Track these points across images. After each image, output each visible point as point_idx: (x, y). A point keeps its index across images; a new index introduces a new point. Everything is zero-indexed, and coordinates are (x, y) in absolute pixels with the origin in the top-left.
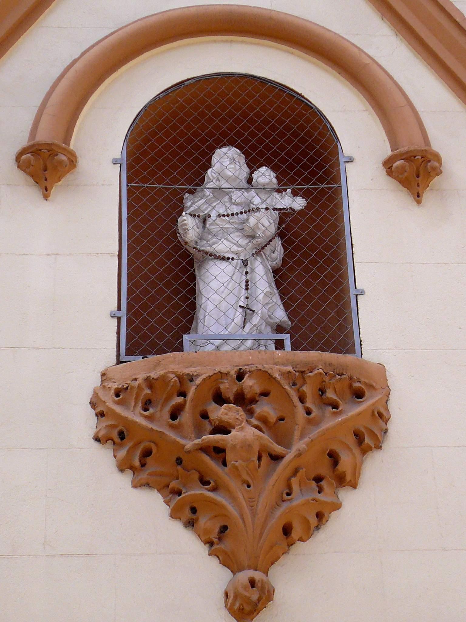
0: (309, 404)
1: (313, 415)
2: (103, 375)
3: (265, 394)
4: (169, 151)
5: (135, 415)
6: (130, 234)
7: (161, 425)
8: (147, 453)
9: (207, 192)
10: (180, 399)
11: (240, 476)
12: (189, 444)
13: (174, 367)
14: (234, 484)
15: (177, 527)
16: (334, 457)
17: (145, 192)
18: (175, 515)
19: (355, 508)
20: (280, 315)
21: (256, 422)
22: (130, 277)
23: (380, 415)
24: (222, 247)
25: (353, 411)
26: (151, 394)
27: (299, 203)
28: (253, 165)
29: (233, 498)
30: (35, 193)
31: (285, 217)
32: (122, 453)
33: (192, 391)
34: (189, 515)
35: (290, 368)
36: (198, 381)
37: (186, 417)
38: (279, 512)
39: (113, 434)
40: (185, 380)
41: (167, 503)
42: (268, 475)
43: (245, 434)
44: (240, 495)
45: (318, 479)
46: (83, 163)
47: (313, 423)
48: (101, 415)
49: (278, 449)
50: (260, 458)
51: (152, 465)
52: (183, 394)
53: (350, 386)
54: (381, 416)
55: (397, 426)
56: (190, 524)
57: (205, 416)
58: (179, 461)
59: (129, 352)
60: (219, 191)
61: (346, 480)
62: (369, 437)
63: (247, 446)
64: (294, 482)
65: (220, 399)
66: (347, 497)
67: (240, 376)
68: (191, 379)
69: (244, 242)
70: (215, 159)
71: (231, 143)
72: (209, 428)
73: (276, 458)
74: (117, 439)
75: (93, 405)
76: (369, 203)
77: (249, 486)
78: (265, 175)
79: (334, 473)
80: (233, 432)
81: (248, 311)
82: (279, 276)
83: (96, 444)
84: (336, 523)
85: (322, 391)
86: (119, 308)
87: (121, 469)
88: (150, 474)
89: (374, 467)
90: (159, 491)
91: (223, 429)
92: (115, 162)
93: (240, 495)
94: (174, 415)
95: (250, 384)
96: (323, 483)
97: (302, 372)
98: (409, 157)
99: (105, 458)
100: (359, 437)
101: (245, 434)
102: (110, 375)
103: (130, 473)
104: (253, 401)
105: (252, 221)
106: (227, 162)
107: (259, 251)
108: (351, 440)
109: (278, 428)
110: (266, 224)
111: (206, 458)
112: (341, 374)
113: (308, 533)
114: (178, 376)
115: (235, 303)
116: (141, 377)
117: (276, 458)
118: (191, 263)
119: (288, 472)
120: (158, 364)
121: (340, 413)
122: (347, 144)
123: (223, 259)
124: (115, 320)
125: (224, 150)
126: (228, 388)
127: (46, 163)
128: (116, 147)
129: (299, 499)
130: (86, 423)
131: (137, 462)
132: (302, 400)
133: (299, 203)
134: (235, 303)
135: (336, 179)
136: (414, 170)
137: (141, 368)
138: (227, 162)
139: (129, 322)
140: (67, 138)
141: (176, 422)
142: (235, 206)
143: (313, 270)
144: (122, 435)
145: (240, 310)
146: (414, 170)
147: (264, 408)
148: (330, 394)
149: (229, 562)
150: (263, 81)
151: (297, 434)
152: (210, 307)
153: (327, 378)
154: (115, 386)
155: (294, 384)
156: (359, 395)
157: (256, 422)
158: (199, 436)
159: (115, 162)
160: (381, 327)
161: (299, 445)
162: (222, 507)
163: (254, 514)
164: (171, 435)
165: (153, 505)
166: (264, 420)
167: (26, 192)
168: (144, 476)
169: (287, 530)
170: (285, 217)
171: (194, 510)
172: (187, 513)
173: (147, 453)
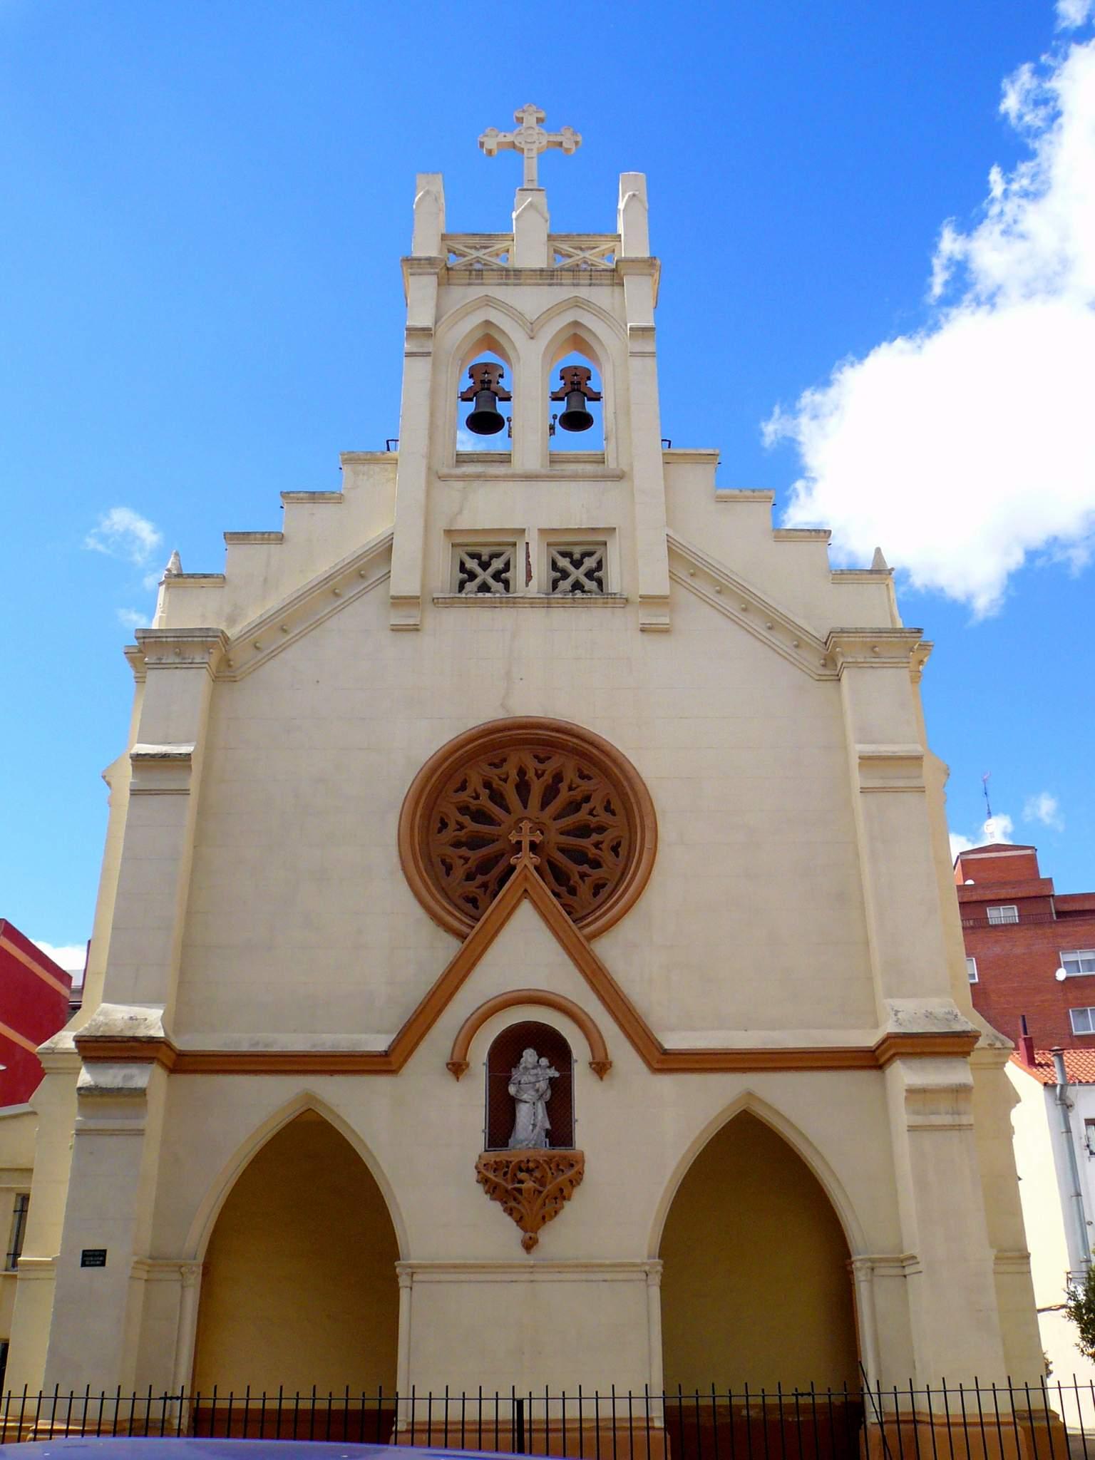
5: (491, 1175)
7: (499, 1180)
15: (505, 1215)
19: (570, 1209)
20: (548, 1126)
24: (525, 1097)
26: (497, 1167)
27: (557, 1075)
28: (540, 1056)
34: (510, 1211)
37: (509, 1176)
39: (484, 1181)
40: (508, 1163)
43: (529, 1185)
46: (472, 1065)
54: (581, 1173)
56: (511, 1214)
60: (526, 1068)
62: (576, 1181)
65: (522, 1171)
66: (567, 1204)
73: (540, 1192)
79: (561, 1196)
81: (534, 1125)
84: (562, 1214)
87: (487, 1193)
89: (578, 1193)
91: (521, 1182)
95: (531, 1165)
98: (598, 1064)
99: (480, 1189)
100: (571, 1181)
101: (529, 1185)
106: (529, 1056)
110: (543, 1085)
113: (551, 1218)
115: (530, 1119)
117: (540, 1192)
122: (575, 1055)
126: (524, 1166)
130: (473, 1175)
133: (557, 1075)
134: (530, 1119)
136: (601, 1067)
137: (493, 1156)
138: (529, 1056)
142: (532, 1072)
143: (560, 1102)
146: (601, 1067)
147: (537, 1174)
149: (525, 1229)
156: (572, 1165)
160: (583, 1137)
161: (549, 1187)
165: (497, 1207)
167: (450, 1077)
169: (544, 1218)
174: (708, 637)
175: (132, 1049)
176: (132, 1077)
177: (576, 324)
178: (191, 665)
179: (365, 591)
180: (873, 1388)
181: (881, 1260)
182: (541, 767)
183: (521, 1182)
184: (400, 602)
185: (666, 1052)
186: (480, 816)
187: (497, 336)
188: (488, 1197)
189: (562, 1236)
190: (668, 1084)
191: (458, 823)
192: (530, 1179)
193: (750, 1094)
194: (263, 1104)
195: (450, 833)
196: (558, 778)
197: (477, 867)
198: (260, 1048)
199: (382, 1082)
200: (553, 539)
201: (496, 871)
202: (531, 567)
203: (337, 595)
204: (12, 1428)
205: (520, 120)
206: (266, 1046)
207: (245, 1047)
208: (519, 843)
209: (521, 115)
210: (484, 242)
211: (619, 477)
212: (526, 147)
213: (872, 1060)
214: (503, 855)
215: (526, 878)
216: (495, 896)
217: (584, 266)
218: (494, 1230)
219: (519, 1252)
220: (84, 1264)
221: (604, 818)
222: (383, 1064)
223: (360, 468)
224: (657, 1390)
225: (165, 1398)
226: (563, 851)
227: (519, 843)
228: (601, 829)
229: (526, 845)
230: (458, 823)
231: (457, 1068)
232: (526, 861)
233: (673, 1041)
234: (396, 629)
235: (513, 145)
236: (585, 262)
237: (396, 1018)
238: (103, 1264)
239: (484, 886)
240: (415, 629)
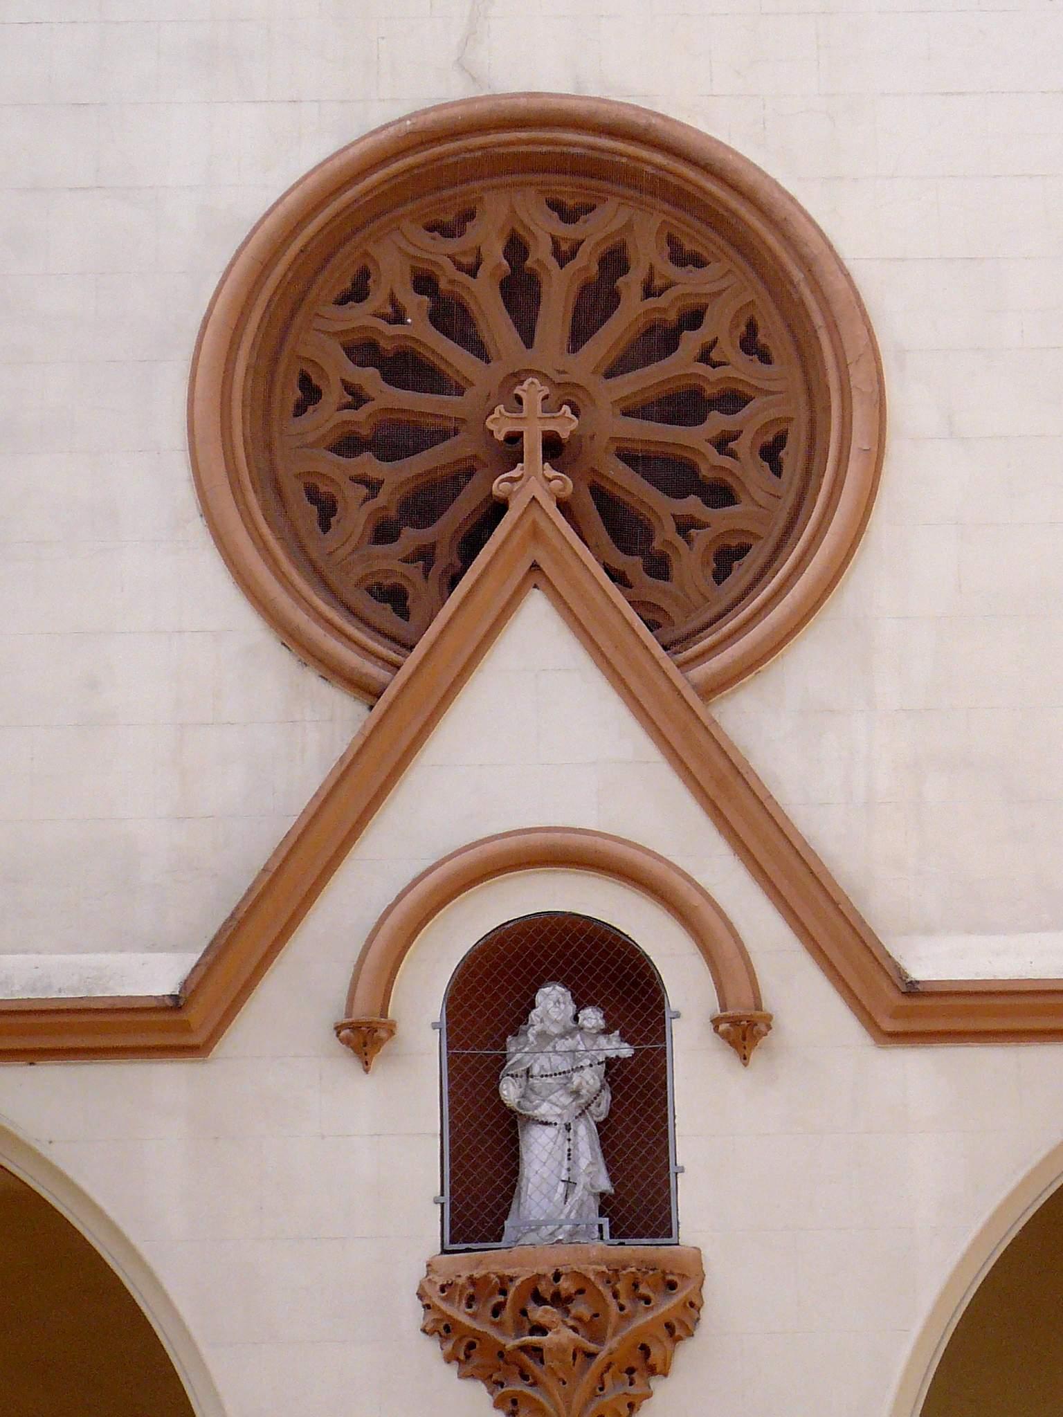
0: (623, 1301)
1: (626, 1311)
2: (428, 1265)
3: (581, 1291)
4: (492, 994)
5: (460, 1314)
6: (453, 1174)
8: (471, 1346)
9: (531, 1038)
10: (501, 1298)
11: (555, 1374)
12: (511, 1343)
13: (495, 1268)
14: (551, 1383)
16: (645, 1349)
17: (466, 1060)
20: (605, 1184)
21: (571, 1323)
22: (452, 1159)
23: (692, 1305)
24: (544, 1110)
25: (666, 1306)
26: (477, 1291)
27: (626, 1051)
28: (581, 1002)
29: (549, 1394)
30: (354, 1065)
31: (612, 1066)
32: (449, 1346)
33: (512, 1291)
35: (604, 1268)
36: (518, 1282)
37: (507, 1314)
38: (593, 1407)
39: (442, 1329)
41: (491, 1393)
42: (583, 1372)
43: (561, 1336)
44: (557, 1393)
45: (630, 1371)
46: (401, 1029)
47: (626, 1319)
48: (427, 1307)
49: (592, 1347)
50: (574, 1358)
51: (476, 1360)
52: (504, 1292)
53: (664, 1278)
54: (693, 1305)
55: (709, 1314)
57: (524, 1312)
58: (501, 1354)
59: (452, 1241)
60: (543, 1036)
62: (679, 1328)
63: (561, 1349)
64: (607, 1377)
65: (539, 1299)
66: (656, 1383)
67: (557, 1276)
68: (511, 1279)
69: (566, 1100)
70: (539, 998)
71: (555, 979)
72: (528, 1327)
73: (591, 1355)
74: (443, 1332)
75: (420, 1296)
76: (695, 1067)
77: (564, 1383)
78: (592, 1017)
80: (550, 1335)
81: (570, 1184)
82: (605, 1130)
83: (423, 1335)
85: (636, 1286)
86: (442, 1195)
87: (449, 1359)
88: (477, 1367)
89: (686, 1356)
90: (483, 1381)
91: (541, 1330)
92: (434, 1026)
93: (557, 1393)
94: (497, 1311)
95: (566, 1285)
96: (635, 1375)
97: (616, 1271)
98: (734, 1021)
99: (432, 1349)
100: (669, 1326)
101: (561, 1336)
102: (434, 1267)
103: (455, 1365)
104: (569, 1299)
105: (576, 1079)
106: (552, 1002)
107: (584, 1112)
108: (662, 1333)
109: (594, 1328)
111: (525, 1357)
112: (653, 1270)
114: (498, 1277)
115: (559, 1168)
116: (465, 1274)
117: (591, 1355)
118: (514, 1125)
119: (600, 1370)
120: (479, 1263)
121: (652, 1308)
123: (546, 1124)
124: (439, 1206)
125: (547, 990)
126: (545, 1289)
127: (365, 1037)
128: (435, 1009)
129: (610, 1395)
130: (412, 1315)
131: (462, 1357)
132: (616, 1295)
133: (626, 1051)
134: (559, 1168)
135: (662, 1038)
136: (743, 1031)
137: (464, 1266)
138: (552, 1002)
139: (453, 1208)
140: (384, 1013)
141: (498, 1319)
142: (561, 1044)
143: (635, 1118)
144: (447, 1328)
145: (562, 1184)
146: (743, 1031)
147: (581, 1308)
148: (643, 1290)
151: (610, 1331)
152: (534, 1180)
153: (639, 1275)
154: (441, 1281)
155: (608, 1282)
156: (672, 1286)
157: (571, 1323)
158: (518, 1337)
159: (434, 1026)
161: (612, 1343)
162: (538, 1402)
163: (569, 1408)
164: (493, 1332)
166: (579, 1319)
167: (348, 1064)
168: (469, 1368)
170: (612, 1066)
171: (514, 1402)
172: (509, 1406)
173: (471, 1346)
183: (541, 1330)
185: (913, 990)
188: (452, 1370)
195: (328, 415)
208: (514, 438)
215: (536, 534)
227: (514, 438)
229: (533, 445)
231: (365, 1037)
233: (929, 961)
237: (203, 912)
239: (425, 555)
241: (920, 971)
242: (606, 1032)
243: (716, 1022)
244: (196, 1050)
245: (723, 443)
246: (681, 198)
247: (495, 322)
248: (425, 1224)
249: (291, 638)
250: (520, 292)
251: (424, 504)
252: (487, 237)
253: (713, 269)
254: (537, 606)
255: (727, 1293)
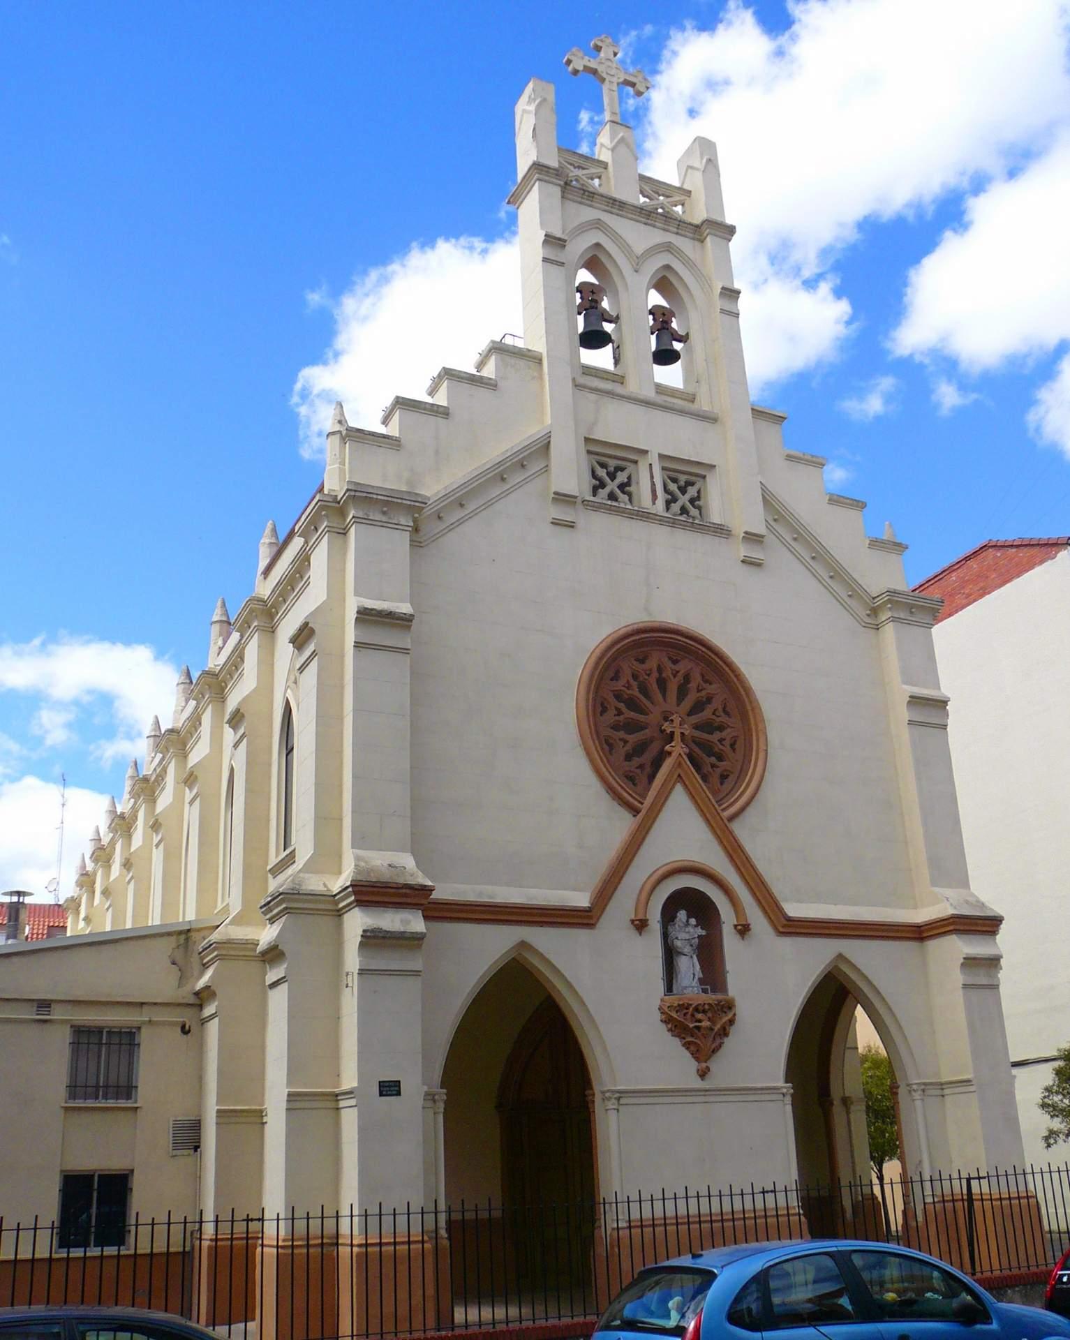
5: (674, 1015)
12: (691, 1025)
18: (683, 1045)
27: (704, 933)
28: (689, 917)
34: (687, 1045)
37: (688, 1016)
39: (668, 1020)
43: (706, 1024)
61: (726, 1035)
66: (726, 1040)
91: (700, 1021)
99: (663, 1027)
126: (701, 1008)
133: (704, 933)
136: (743, 930)
143: (710, 953)
146: (743, 930)
147: (710, 1014)
149: (697, 1059)
150: (709, 898)
160: (735, 986)
165: (676, 1042)
167: (634, 933)
174: (789, 579)
175: (406, 895)
176: (408, 922)
177: (598, 245)
178: (396, 527)
179: (526, 481)
180: (133, 1222)
181: (931, 1084)
182: (676, 667)
183: (700, 1021)
184: (562, 498)
185: (789, 919)
186: (632, 704)
187: (603, 259)
188: (669, 1034)
189: (726, 1067)
190: (789, 945)
191: (617, 709)
192: (701, 1025)
193: (840, 957)
194: (486, 948)
195: (610, 717)
196: (687, 678)
197: (634, 749)
198: (486, 900)
199: (581, 934)
200: (667, 465)
201: (648, 757)
202: (647, 485)
203: (503, 479)
204: (300, 1246)
205: (598, 48)
206: (491, 897)
207: (472, 898)
208: (673, 733)
209: (599, 44)
210: (582, 162)
211: (711, 419)
212: (608, 78)
213: (920, 933)
214: (652, 741)
215: (680, 764)
216: (651, 778)
217: (660, 211)
218: (670, 1062)
219: (697, 1083)
220: (381, 1094)
221: (723, 718)
222: (582, 919)
223: (508, 359)
224: (442, 1206)
225: (763, 1192)
226: (694, 742)
227: (673, 733)
228: (721, 728)
229: (677, 736)
230: (617, 709)
231: (640, 925)
232: (677, 749)
233: (794, 910)
234: (556, 523)
235: (594, 72)
236: (577, 180)
237: (595, 878)
238: (399, 1094)
239: (641, 767)
240: (571, 525)
241: (791, 914)
242: (696, 926)
243: (735, 926)
244: (591, 926)
245: (721, 741)
246: (709, 663)
247: (687, 704)
248: (660, 986)
249: (610, 789)
250: (662, 684)
251: (640, 749)
252: (652, 663)
253: (713, 686)
254: (679, 788)
255: (744, 1009)
